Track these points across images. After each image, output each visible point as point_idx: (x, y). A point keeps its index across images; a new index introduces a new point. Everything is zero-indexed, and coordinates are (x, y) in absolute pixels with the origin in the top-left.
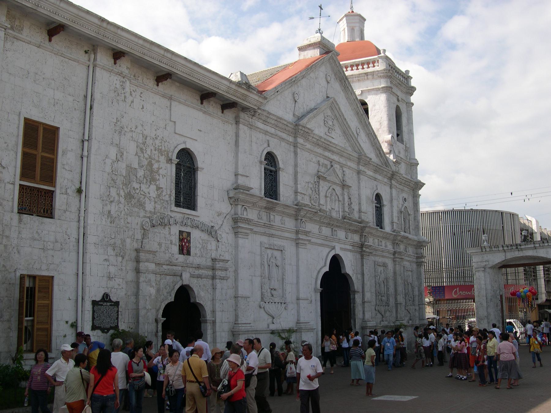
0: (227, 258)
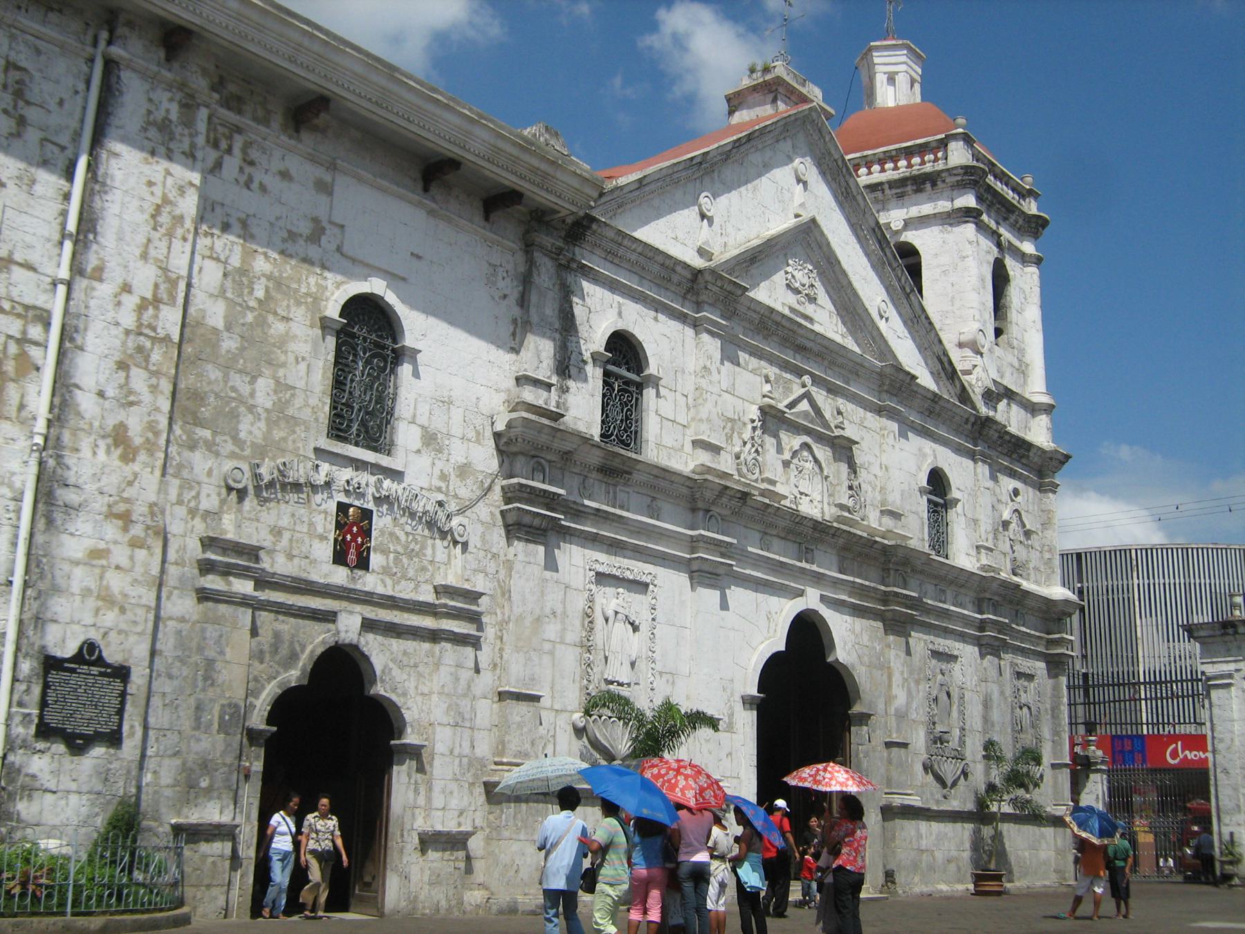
0: (479, 589)
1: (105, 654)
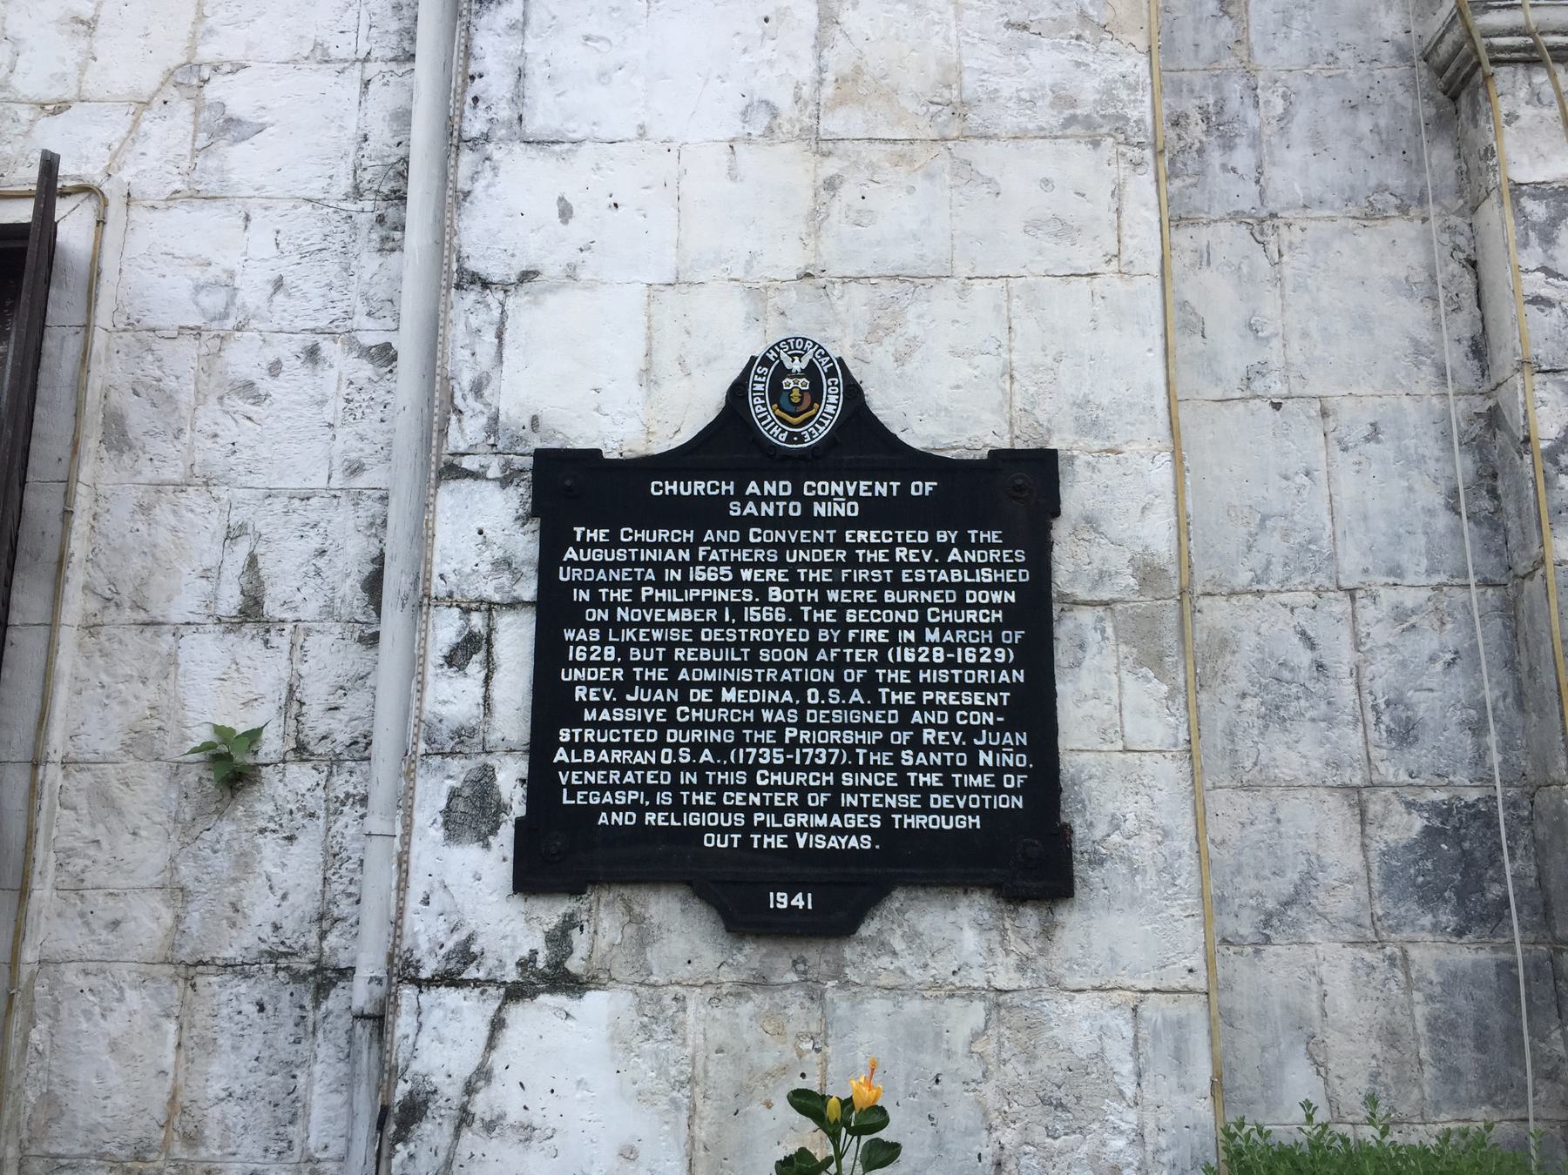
1: (885, 405)
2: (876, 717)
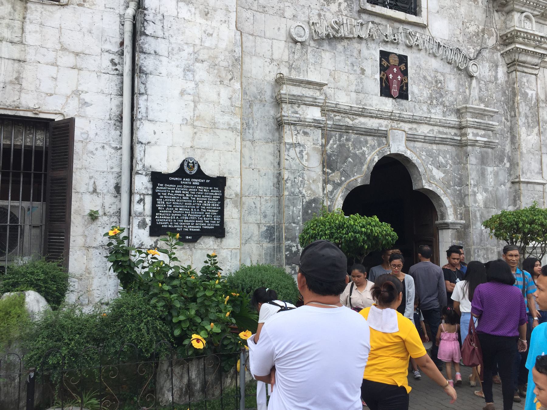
1: (202, 168)
2: (201, 213)
